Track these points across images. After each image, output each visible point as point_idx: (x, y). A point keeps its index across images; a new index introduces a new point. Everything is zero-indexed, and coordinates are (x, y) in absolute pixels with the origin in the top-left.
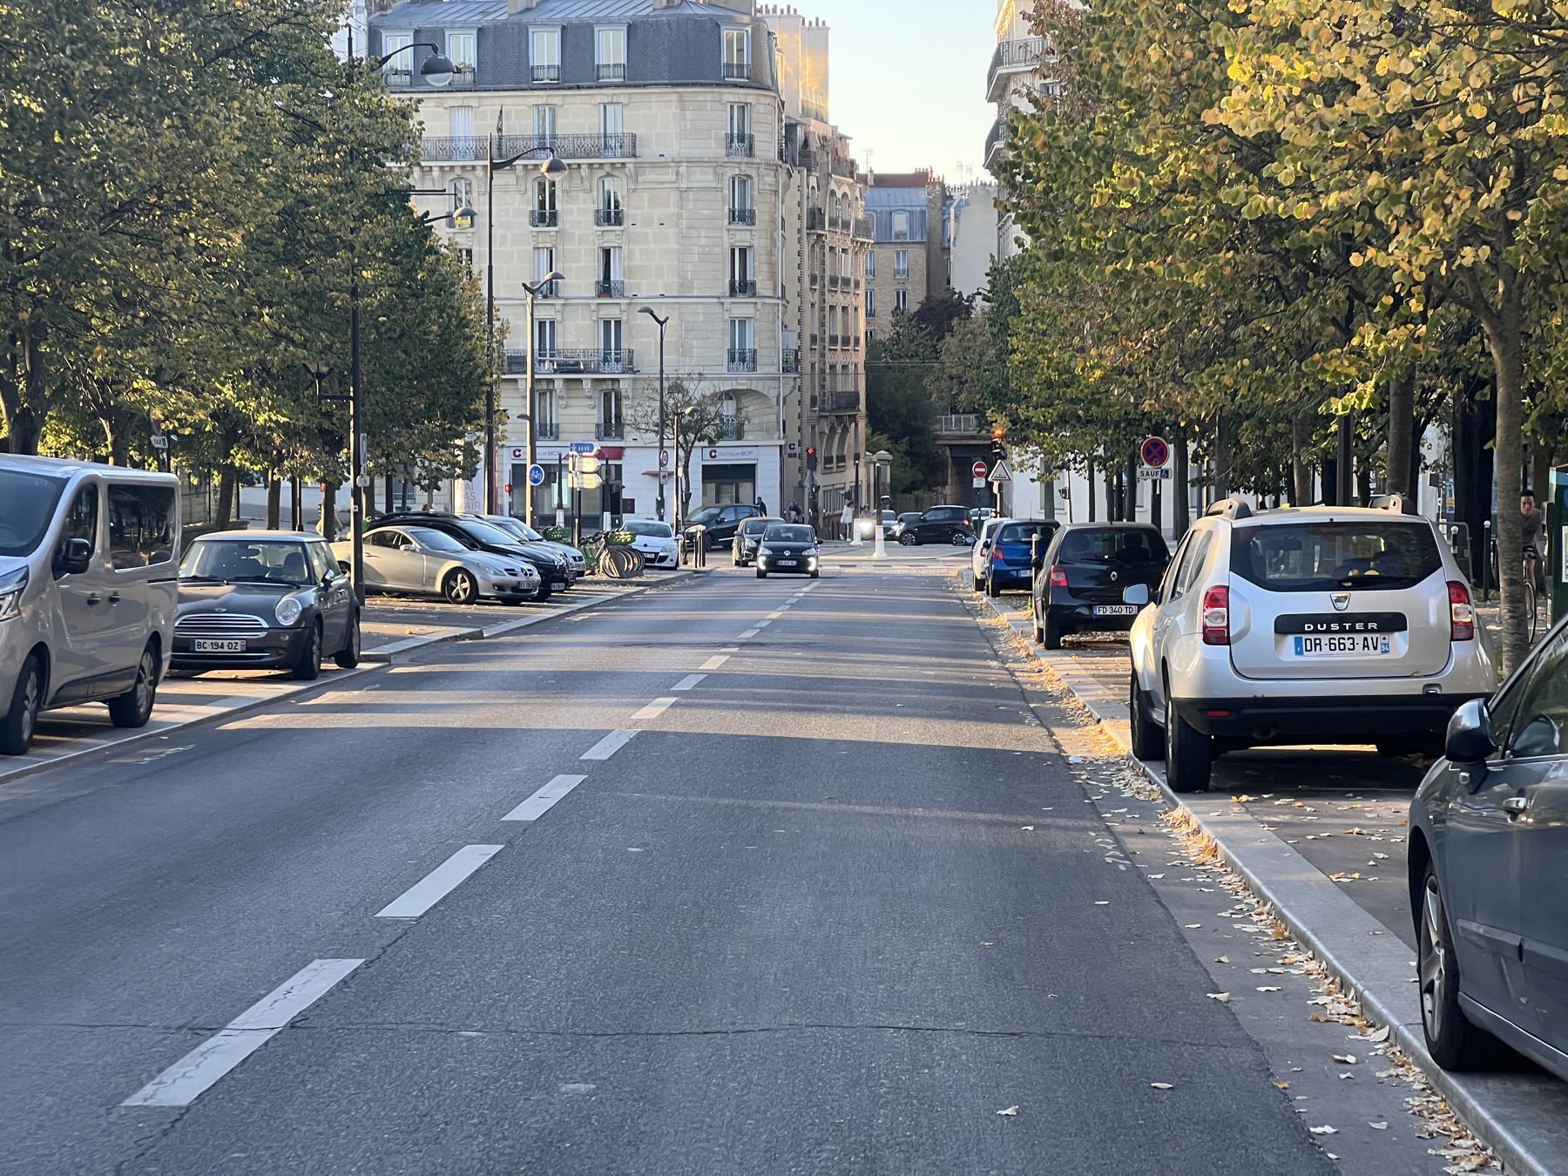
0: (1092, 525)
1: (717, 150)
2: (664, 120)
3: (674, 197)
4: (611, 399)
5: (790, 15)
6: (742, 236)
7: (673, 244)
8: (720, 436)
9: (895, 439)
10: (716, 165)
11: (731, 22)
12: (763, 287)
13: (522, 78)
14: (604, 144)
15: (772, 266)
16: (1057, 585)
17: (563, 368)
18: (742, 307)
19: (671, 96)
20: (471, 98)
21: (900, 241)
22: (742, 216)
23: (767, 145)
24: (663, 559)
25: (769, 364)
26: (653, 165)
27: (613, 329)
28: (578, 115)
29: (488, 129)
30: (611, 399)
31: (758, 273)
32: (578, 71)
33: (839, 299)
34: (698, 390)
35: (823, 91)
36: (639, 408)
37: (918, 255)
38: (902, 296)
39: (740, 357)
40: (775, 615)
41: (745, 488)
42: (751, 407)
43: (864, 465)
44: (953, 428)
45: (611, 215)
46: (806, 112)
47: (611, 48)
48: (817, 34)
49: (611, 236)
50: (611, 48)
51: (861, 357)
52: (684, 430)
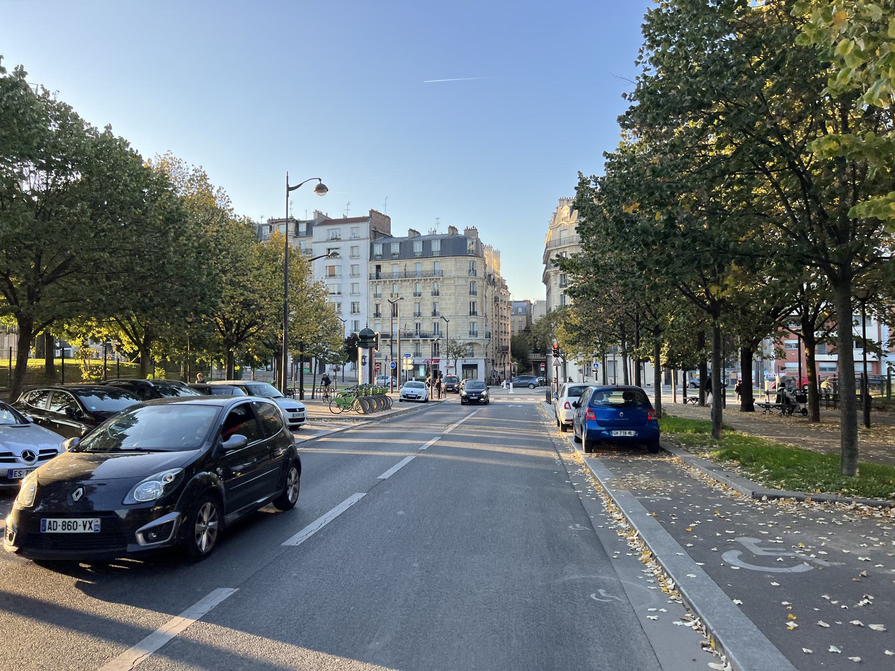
0: (605, 387)
1: (466, 274)
2: (449, 265)
3: (453, 287)
4: (436, 345)
5: (490, 247)
6: (473, 299)
7: (453, 301)
8: (466, 355)
9: (518, 359)
10: (466, 278)
11: (470, 238)
12: (479, 313)
13: (412, 256)
14: (434, 273)
15: (482, 307)
16: (590, 418)
17: (421, 337)
18: (473, 319)
19: (453, 259)
20: (398, 262)
21: (520, 315)
22: (473, 293)
23: (480, 274)
24: (419, 397)
25: (481, 336)
26: (448, 279)
27: (436, 325)
28: (427, 265)
29: (402, 269)
30: (436, 345)
31: (478, 309)
32: (427, 253)
33: (503, 321)
34: (460, 342)
35: (499, 268)
36: (443, 349)
37: (525, 317)
38: (521, 327)
39: (473, 333)
40: (431, 443)
41: (475, 371)
42: (476, 348)
43: (510, 365)
44: (533, 357)
45: (436, 294)
46: (494, 272)
47: (436, 247)
48: (497, 254)
49: (436, 299)
50: (436, 247)
51: (509, 337)
52: (455, 353)
